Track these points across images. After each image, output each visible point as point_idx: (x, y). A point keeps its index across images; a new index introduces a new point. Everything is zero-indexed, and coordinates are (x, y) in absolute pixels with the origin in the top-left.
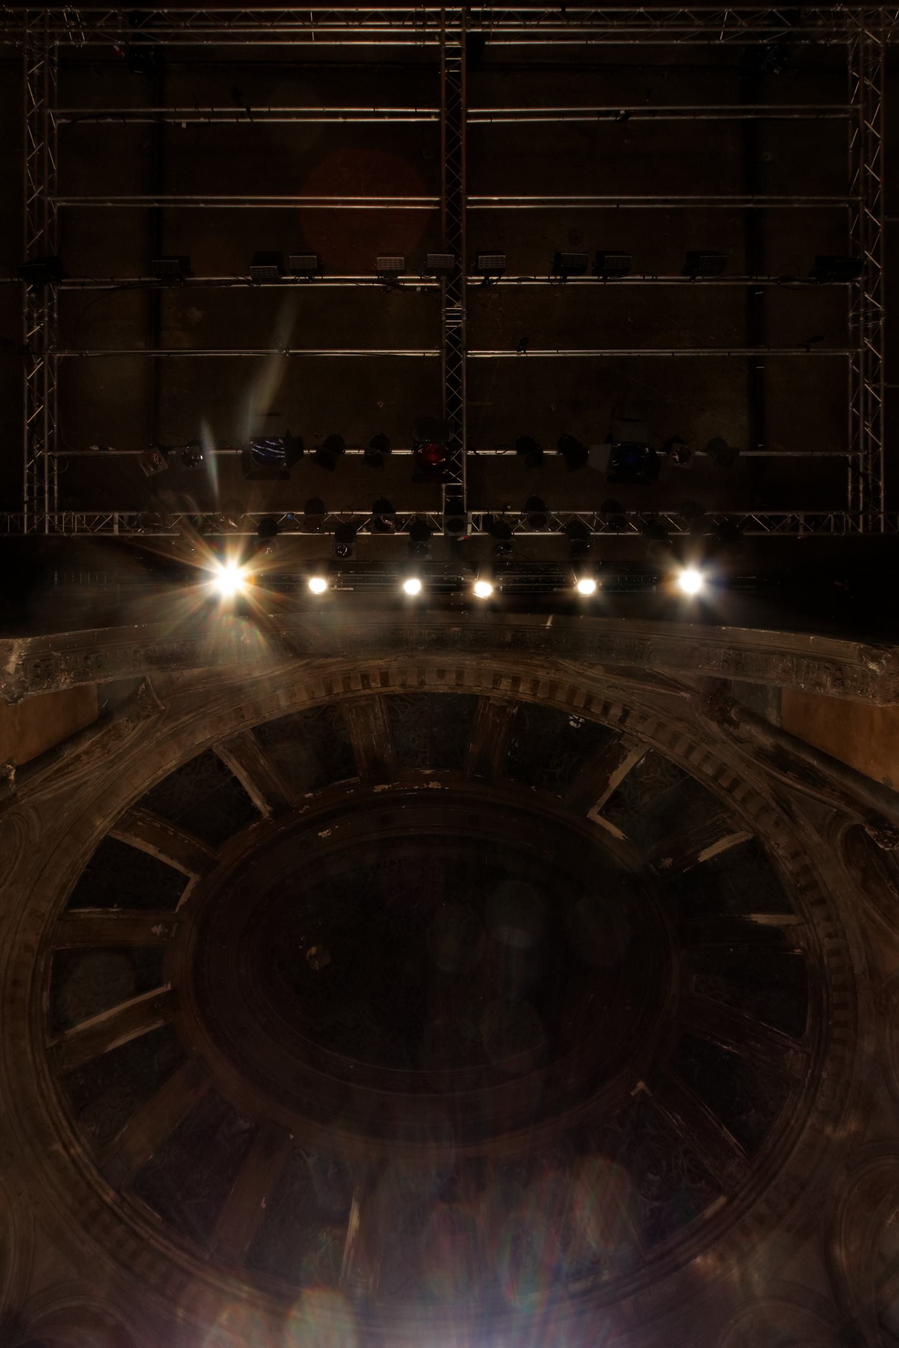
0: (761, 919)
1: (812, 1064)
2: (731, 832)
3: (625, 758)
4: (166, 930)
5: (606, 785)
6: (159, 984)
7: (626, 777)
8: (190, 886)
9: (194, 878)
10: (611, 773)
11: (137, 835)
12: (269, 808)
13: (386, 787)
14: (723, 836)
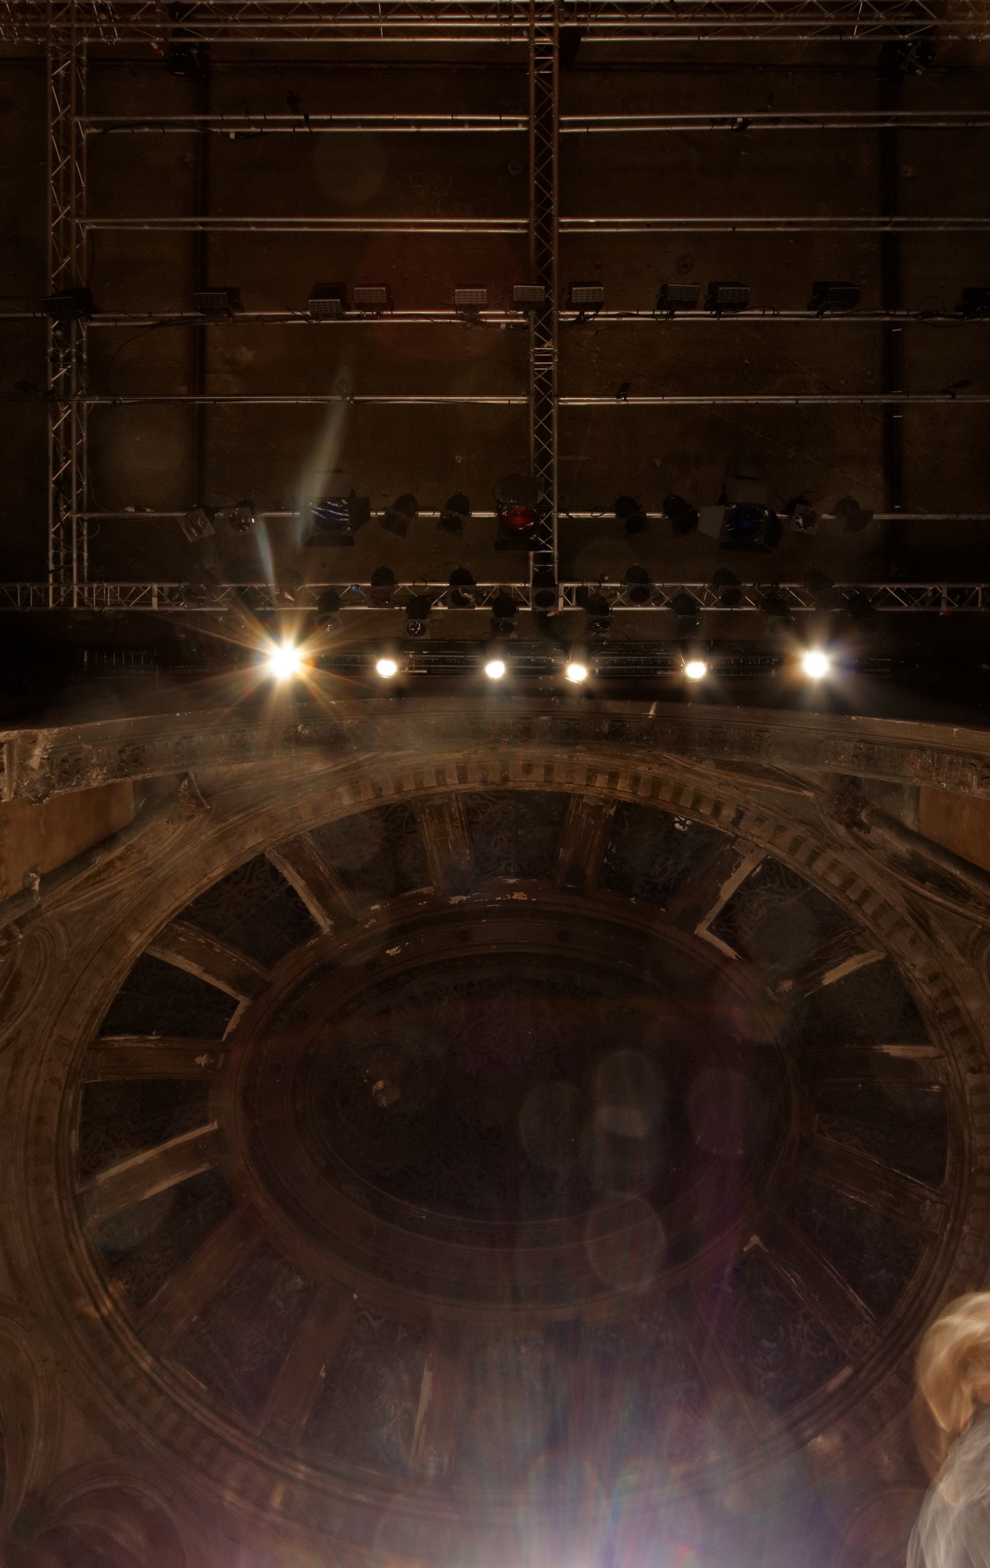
0: (894, 1050)
1: (951, 1217)
2: (860, 951)
3: (738, 866)
4: (212, 1061)
5: (716, 897)
6: (204, 1122)
7: (740, 887)
8: (239, 1011)
9: (243, 1002)
10: (722, 883)
11: (178, 953)
12: (330, 922)
13: (464, 898)
14: (851, 955)
